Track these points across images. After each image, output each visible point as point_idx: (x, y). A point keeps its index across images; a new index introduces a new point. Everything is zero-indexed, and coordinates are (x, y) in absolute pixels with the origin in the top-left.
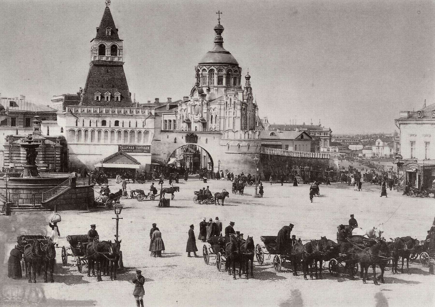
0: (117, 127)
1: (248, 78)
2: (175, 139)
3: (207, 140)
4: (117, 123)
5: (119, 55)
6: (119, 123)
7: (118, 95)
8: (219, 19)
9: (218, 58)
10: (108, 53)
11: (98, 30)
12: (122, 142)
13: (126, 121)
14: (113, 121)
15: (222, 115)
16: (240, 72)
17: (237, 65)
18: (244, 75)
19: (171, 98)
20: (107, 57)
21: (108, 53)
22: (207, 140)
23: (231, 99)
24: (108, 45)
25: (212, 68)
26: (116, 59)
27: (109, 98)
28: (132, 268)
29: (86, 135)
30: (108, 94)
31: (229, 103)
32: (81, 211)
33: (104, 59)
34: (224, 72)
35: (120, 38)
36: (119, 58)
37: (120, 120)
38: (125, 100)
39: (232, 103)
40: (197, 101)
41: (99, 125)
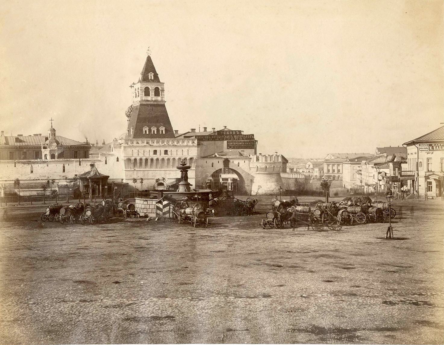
0: (166, 155)
2: (213, 164)
4: (166, 152)
6: (168, 152)
7: (162, 129)
10: (152, 93)
13: (174, 149)
14: (163, 150)
19: (178, 131)
20: (152, 97)
21: (152, 93)
24: (152, 87)
26: (159, 98)
27: (164, 132)
29: (168, 163)
32: (242, 231)
33: (149, 98)
35: (161, 81)
36: (162, 98)
37: (169, 149)
38: (170, 133)
41: (152, 153)
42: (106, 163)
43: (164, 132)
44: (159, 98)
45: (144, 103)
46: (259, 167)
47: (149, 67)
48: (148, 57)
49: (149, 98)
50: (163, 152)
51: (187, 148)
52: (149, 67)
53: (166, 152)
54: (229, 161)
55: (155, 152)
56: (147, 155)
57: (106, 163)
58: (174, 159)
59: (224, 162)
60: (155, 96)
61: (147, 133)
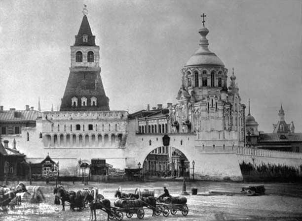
1: (233, 79)
3: (150, 141)
4: (91, 127)
5: (96, 61)
7: (94, 100)
8: (204, 22)
10: (85, 59)
11: (70, 68)
16: (225, 73)
18: (229, 74)
20: (85, 63)
21: (85, 59)
22: (150, 141)
23: (212, 100)
24: (85, 50)
26: (92, 65)
30: (84, 100)
31: (210, 103)
34: (209, 73)
39: (214, 103)
41: (74, 128)
42: (28, 140)
43: (76, 103)
45: (77, 70)
46: (205, 146)
47: (85, 28)
48: (84, 17)
50: (87, 128)
51: (115, 123)
52: (85, 28)
53: (91, 127)
54: (169, 138)
55: (78, 127)
56: (68, 131)
57: (28, 140)
58: (62, 136)
59: (164, 139)
60: (88, 61)
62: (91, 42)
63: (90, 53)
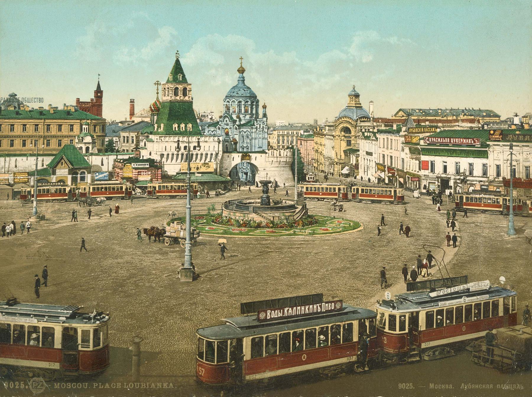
1: (264, 107)
8: (241, 63)
9: (353, 93)
10: (180, 93)
12: (478, 163)
15: (253, 137)
17: (256, 97)
18: (261, 104)
21: (180, 93)
24: (180, 87)
25: (241, 100)
26: (187, 98)
28: (469, 262)
31: (258, 127)
33: (178, 98)
34: (249, 103)
36: (189, 97)
39: (261, 127)
40: (227, 125)
44: (187, 98)
47: (178, 69)
49: (178, 98)
61: (177, 129)
62: (184, 80)
63: (185, 89)
